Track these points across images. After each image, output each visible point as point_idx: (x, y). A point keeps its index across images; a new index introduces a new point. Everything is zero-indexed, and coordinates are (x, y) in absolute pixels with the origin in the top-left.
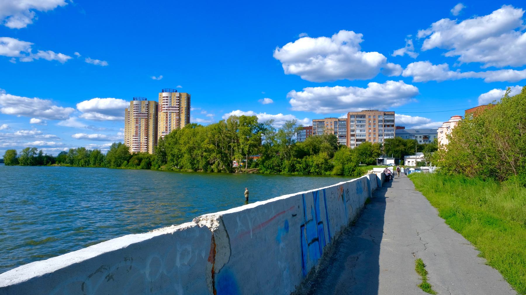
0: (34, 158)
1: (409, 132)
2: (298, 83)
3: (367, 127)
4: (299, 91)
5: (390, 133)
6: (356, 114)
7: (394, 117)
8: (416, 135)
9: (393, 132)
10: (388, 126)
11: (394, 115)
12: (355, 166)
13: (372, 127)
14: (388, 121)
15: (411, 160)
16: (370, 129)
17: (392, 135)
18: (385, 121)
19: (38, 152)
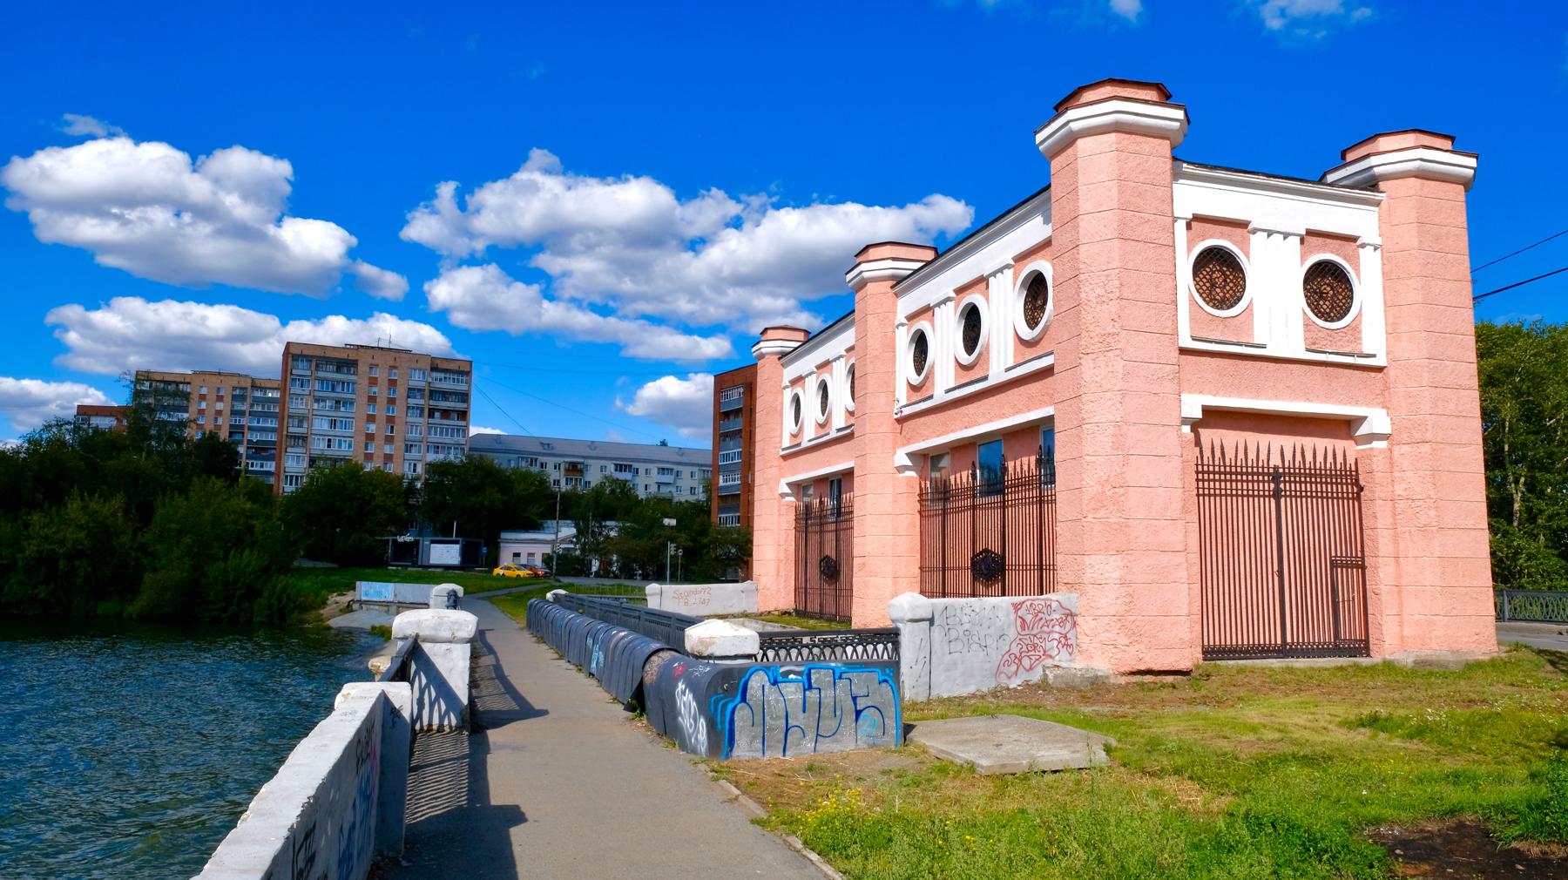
1: (519, 447)
2: (92, 278)
3: (360, 409)
4: (98, 308)
5: (448, 440)
6: (318, 353)
7: (469, 383)
8: (542, 459)
10: (446, 414)
11: (468, 373)
12: (265, 570)
13: (380, 411)
14: (445, 395)
15: (524, 550)
18: (433, 393)
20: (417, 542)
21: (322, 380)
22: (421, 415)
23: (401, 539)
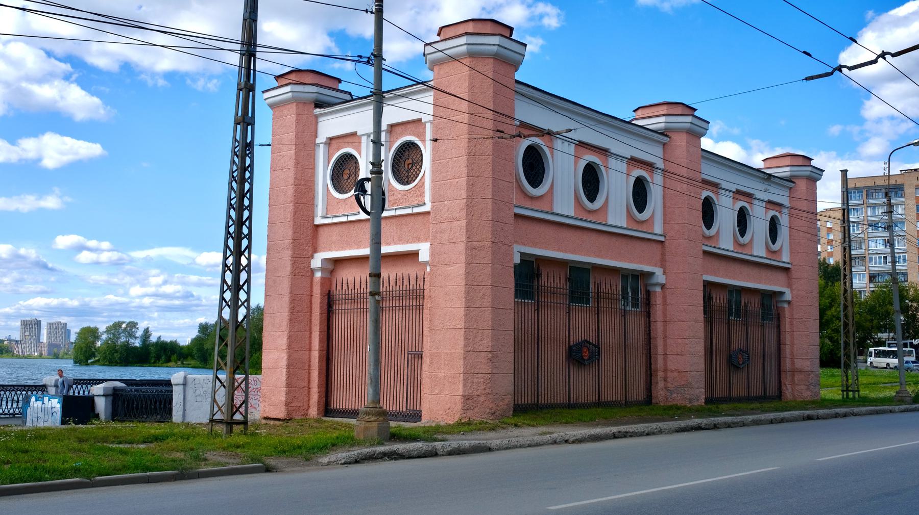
0: (127, 348)
19: (139, 333)
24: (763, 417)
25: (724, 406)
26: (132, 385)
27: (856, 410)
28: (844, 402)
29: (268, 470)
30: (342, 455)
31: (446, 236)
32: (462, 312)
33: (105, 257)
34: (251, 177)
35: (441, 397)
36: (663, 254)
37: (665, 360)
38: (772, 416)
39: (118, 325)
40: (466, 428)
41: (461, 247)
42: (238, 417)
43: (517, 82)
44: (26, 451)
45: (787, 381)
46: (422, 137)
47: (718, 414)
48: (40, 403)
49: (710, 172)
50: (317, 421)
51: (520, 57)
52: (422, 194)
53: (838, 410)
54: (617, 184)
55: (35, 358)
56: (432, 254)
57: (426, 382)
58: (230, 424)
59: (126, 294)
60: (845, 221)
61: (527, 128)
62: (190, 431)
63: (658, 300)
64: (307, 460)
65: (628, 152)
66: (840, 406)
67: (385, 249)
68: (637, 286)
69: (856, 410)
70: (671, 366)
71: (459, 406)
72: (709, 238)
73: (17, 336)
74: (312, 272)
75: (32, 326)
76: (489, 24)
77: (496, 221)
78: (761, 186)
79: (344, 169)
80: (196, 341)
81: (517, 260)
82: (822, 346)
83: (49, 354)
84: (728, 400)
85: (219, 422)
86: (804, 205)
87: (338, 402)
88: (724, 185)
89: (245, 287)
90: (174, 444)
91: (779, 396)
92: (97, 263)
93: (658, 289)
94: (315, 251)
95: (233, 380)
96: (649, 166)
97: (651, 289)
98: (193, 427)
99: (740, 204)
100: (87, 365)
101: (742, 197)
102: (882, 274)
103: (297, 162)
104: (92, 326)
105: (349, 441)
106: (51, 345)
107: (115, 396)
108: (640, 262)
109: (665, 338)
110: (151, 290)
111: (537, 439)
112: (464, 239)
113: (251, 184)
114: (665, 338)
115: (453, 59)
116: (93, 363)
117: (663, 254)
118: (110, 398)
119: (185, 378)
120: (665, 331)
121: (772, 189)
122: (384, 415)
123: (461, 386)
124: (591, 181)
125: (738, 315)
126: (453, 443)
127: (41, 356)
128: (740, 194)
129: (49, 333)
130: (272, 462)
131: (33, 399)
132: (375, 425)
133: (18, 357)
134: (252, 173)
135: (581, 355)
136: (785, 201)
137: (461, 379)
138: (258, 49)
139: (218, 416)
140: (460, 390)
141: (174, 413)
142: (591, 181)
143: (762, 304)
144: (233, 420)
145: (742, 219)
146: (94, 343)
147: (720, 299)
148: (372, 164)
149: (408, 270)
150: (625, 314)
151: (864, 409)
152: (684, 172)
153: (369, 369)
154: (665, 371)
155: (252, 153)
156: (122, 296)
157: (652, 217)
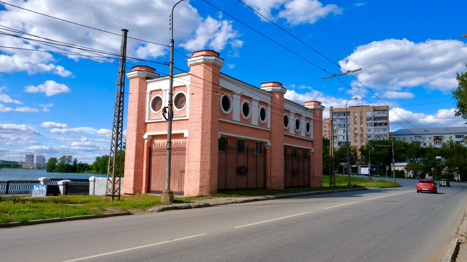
0: (68, 166)
6: (339, 111)
9: (371, 122)
10: (380, 124)
14: (380, 118)
16: (356, 129)
17: (331, 154)
18: (375, 119)
19: (73, 160)
20: (357, 167)
21: (340, 119)
22: (372, 126)
23: (353, 166)
24: (304, 193)
25: (290, 189)
26: (73, 181)
27: (335, 190)
28: (330, 188)
29: (129, 214)
30: (157, 208)
31: (194, 128)
32: (199, 155)
33: (62, 131)
34: (123, 105)
35: (192, 185)
36: (270, 136)
37: (270, 173)
38: (307, 193)
39: (64, 157)
40: (201, 198)
41: (200, 132)
42: (116, 194)
43: (221, 73)
44: (37, 207)
45: (311, 180)
46: (186, 91)
47: (289, 192)
48: (37, 188)
49: (287, 107)
50: (145, 195)
51: (222, 64)
52: (185, 112)
53: (329, 191)
54: (255, 111)
55: (31, 169)
56: (189, 134)
57: (186, 181)
58: (113, 196)
59: (70, 145)
60: (332, 124)
61: (224, 89)
62: (98, 199)
63: (268, 152)
64: (144, 210)
65: (259, 99)
66: (329, 189)
67: (173, 132)
68: (261, 148)
69: (335, 190)
70: (272, 175)
71: (198, 190)
72: (286, 130)
73: (24, 160)
74: (144, 140)
75: (30, 157)
76: (211, 52)
77: (212, 123)
78: (304, 112)
79: (156, 102)
80: (95, 164)
81: (220, 137)
82: (323, 167)
83: (37, 168)
84: (292, 187)
85: (109, 195)
86: (318, 119)
87: (154, 187)
88: (292, 111)
89: (120, 146)
90: (93, 204)
91: (309, 185)
92: (59, 133)
93: (268, 148)
94: (146, 132)
95: (114, 180)
96: (266, 104)
97: (266, 148)
98: (99, 197)
99: (297, 118)
100: (52, 172)
101: (297, 116)
102: (343, 142)
103: (139, 99)
104: (54, 157)
105: (159, 203)
106: (37, 164)
107: (66, 186)
108: (262, 138)
109: (271, 165)
110: (80, 144)
111: (226, 202)
112: (201, 129)
113: (123, 108)
114: (271, 165)
115: (198, 64)
116: (54, 171)
117: (270, 136)
118: (65, 186)
119: (95, 179)
120: (270, 163)
121: (308, 113)
122: (171, 193)
123: (199, 183)
124: (246, 109)
125: (296, 157)
126: (197, 203)
127: (33, 168)
128: (296, 114)
129: (37, 160)
130: (131, 211)
131: (35, 186)
132: (169, 197)
133: (24, 169)
134: (123, 103)
135: (242, 171)
136: (312, 117)
137: (199, 180)
138: (126, 58)
139: (109, 193)
140: (198, 184)
141: (90, 192)
142: (246, 109)
143: (304, 153)
144: (115, 195)
145: (297, 124)
146: (55, 164)
147: (289, 151)
148: (169, 102)
149: (181, 140)
150: (257, 156)
151: (337, 190)
152: (278, 106)
153: (167, 177)
154: (271, 177)
155: (123, 96)
156: (68, 146)
157: (267, 122)
